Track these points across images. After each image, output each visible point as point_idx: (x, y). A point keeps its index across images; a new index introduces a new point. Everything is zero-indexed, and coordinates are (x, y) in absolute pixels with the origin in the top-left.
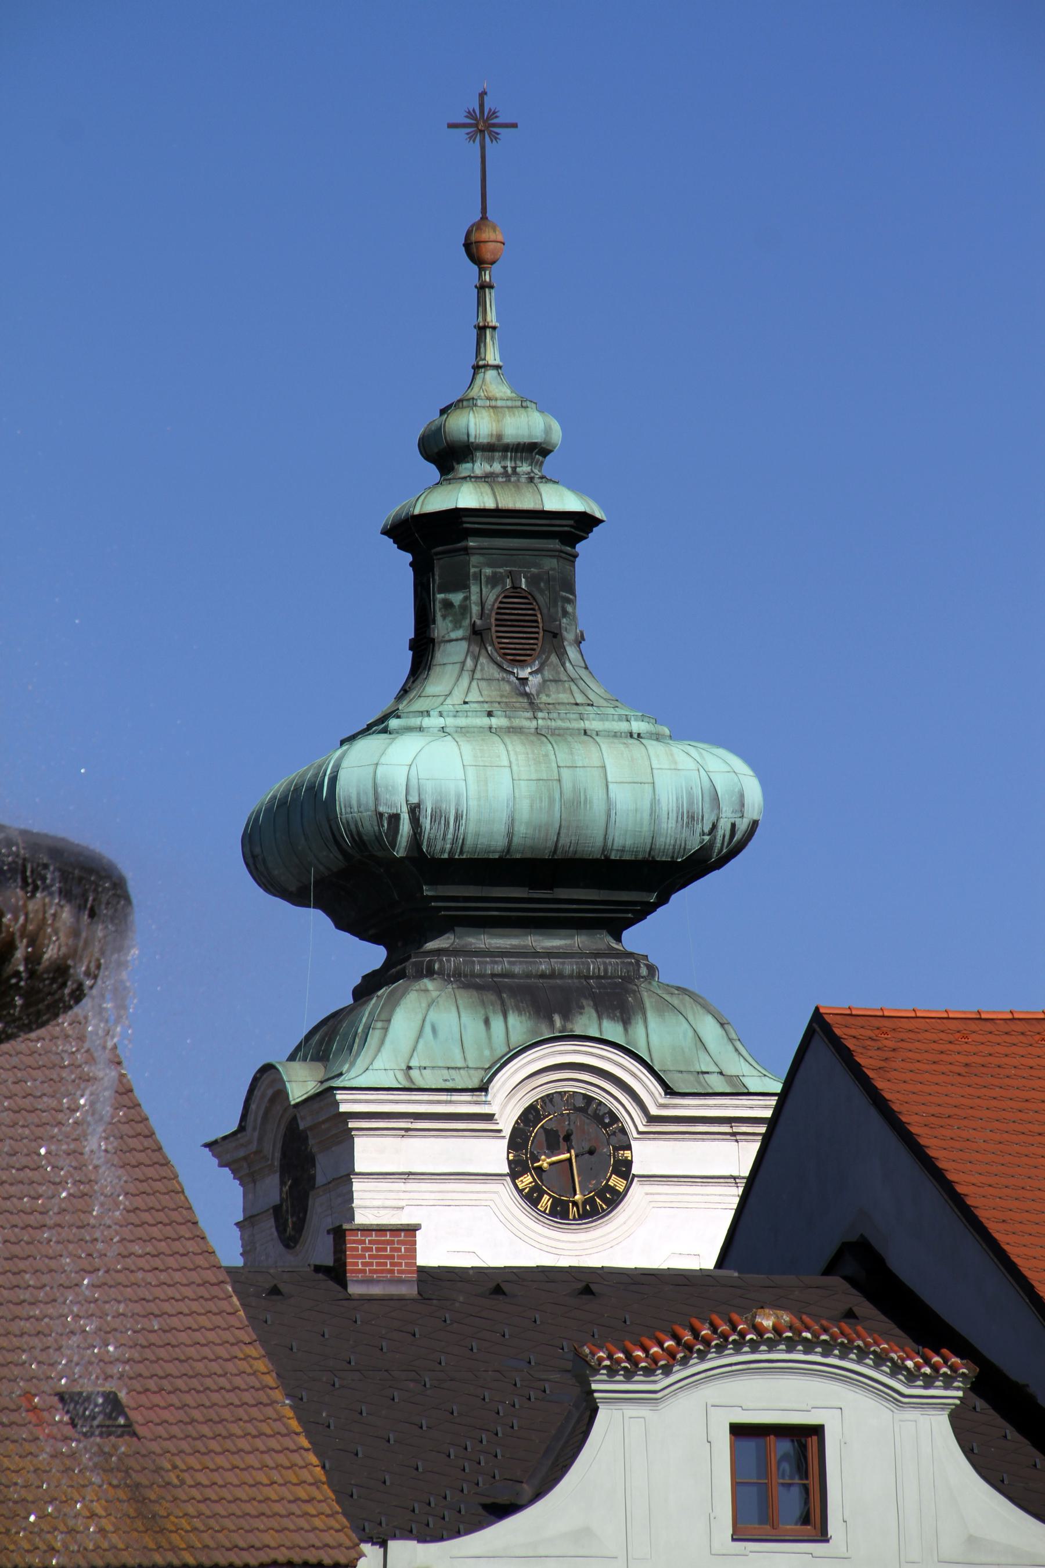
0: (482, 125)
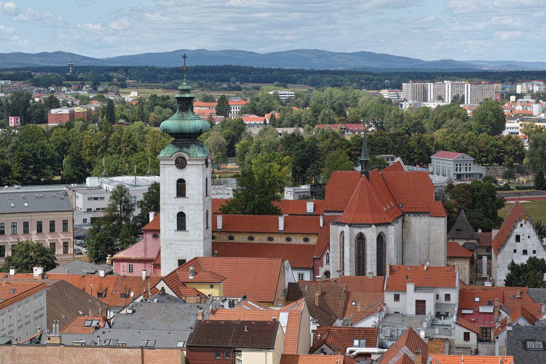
0: (185, 57)
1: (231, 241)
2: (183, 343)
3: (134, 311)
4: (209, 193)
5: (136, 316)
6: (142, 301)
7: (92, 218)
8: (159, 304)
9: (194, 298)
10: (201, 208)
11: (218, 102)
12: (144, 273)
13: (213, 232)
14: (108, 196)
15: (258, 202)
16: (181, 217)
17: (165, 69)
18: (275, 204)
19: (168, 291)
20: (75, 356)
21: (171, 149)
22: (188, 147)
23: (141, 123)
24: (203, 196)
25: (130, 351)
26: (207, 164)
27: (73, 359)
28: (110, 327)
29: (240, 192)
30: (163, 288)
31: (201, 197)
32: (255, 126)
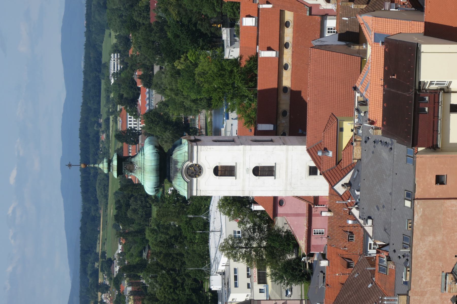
0: (70, 165)
1: (288, 114)
2: (406, 201)
3: (370, 218)
4: (231, 139)
5: (374, 213)
6: (357, 208)
7: (259, 283)
8: (361, 189)
9: (355, 148)
10: (248, 147)
11: (122, 142)
12: (324, 214)
13: (276, 135)
14: (234, 264)
15: (241, 83)
16: (258, 171)
17: (84, 208)
18: (244, 63)
19: (346, 179)
20: (422, 277)
21: (178, 183)
22: (176, 162)
23: (147, 232)
24: (234, 145)
25: (417, 213)
26: (196, 141)
27: (425, 280)
28: (388, 245)
29: (229, 104)
30: (343, 185)
31: (236, 147)
32: (150, 99)
